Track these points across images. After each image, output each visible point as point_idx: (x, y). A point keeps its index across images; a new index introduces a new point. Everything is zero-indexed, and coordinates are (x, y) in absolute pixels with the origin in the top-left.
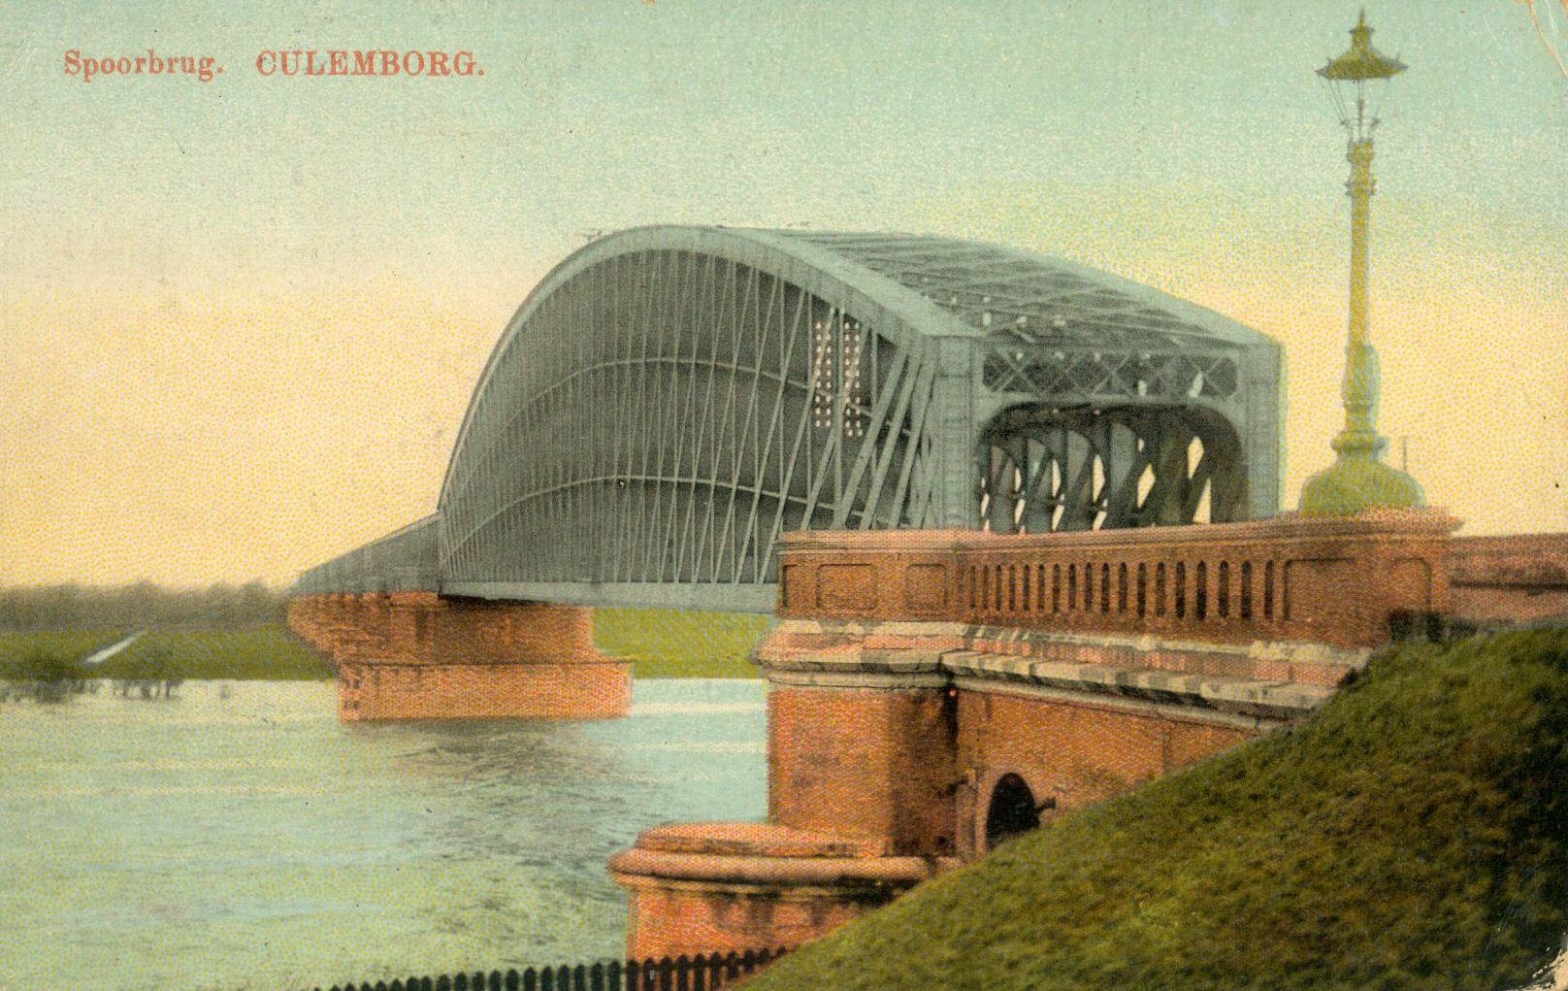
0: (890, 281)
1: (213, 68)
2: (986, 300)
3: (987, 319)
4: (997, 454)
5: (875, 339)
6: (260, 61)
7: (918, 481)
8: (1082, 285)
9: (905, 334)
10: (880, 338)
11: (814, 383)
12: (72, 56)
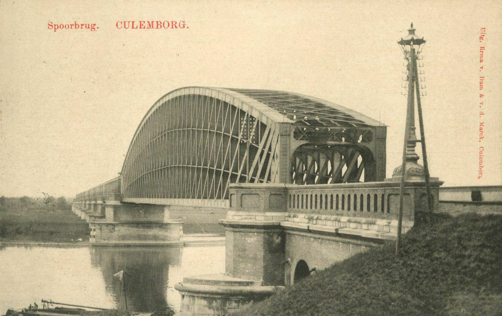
0: (265, 105)
1: (96, 27)
2: (295, 111)
3: (295, 117)
4: (298, 160)
6: (117, 25)
7: (272, 170)
8: (325, 107)
9: (270, 121)
10: (262, 123)
11: (240, 137)
12: (50, 24)
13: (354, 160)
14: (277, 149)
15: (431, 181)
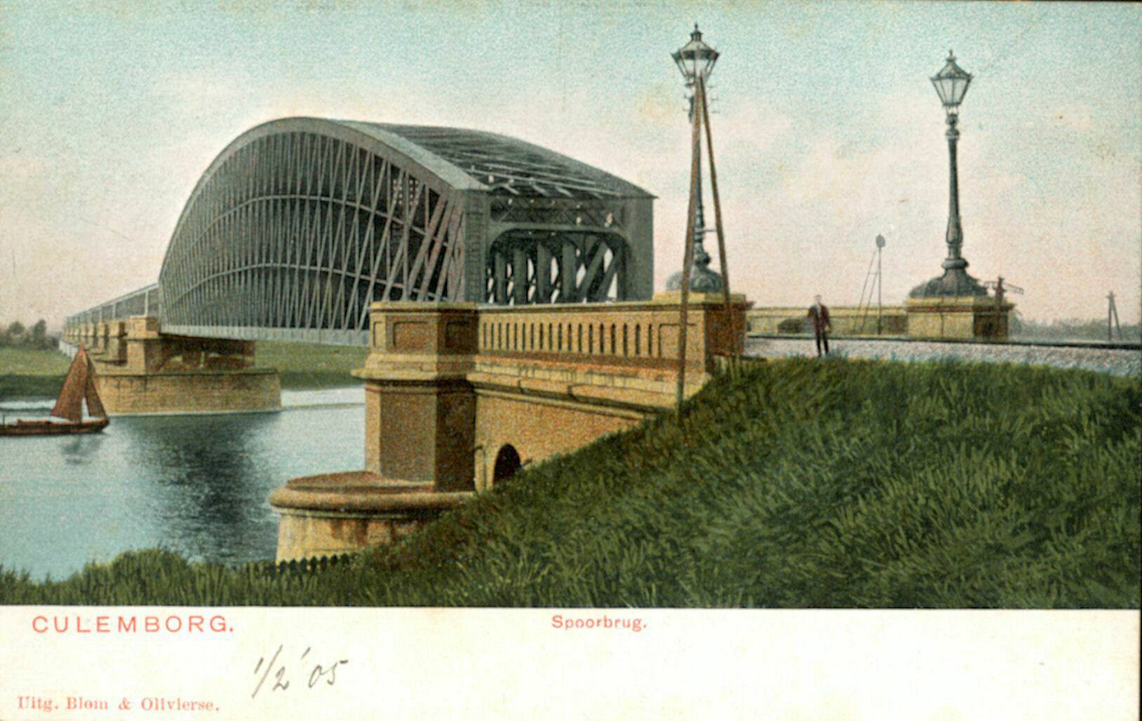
5: (427, 191)
8: (427, 144)
13: (597, 261)
14: (459, 238)
15: (732, 301)
